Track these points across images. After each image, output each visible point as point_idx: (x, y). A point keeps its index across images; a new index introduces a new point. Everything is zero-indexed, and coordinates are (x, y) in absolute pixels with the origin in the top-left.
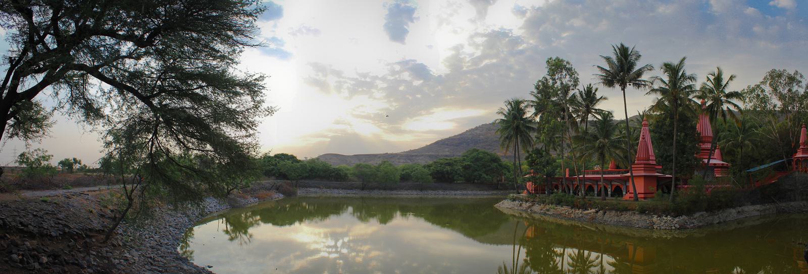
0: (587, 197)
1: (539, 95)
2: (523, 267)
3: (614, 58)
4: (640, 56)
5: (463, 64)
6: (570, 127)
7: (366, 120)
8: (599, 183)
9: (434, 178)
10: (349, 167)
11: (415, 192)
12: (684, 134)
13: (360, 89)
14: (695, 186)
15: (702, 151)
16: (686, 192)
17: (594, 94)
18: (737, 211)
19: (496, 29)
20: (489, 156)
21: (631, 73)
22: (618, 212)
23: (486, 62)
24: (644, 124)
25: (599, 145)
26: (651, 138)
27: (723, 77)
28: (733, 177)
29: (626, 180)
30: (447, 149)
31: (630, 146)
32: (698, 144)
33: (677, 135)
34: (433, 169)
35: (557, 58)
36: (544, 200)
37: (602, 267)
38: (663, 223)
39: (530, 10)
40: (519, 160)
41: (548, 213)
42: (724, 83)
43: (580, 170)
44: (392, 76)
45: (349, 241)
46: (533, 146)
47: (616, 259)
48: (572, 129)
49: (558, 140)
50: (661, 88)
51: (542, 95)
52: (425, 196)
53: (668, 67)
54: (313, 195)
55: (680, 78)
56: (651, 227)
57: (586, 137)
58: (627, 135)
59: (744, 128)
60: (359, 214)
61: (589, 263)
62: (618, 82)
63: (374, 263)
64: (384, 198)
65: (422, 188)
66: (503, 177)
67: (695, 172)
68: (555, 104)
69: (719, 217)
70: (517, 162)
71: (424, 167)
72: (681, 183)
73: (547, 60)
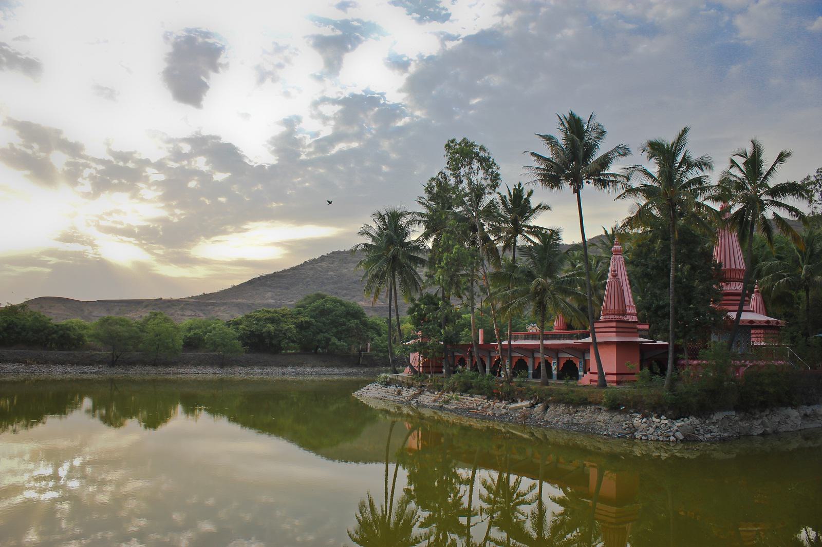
0: (515, 380)
1: (432, 203)
2: (402, 501)
3: (560, 138)
4: (604, 132)
5: (301, 149)
6: (485, 258)
7: (125, 238)
8: (536, 355)
9: (245, 345)
10: (87, 324)
11: (210, 370)
12: (690, 266)
13: (116, 181)
14: (714, 363)
15: (725, 298)
16: (696, 371)
17: (527, 200)
18: (803, 413)
19: (359, 92)
20: (343, 307)
21: (590, 162)
22: (571, 407)
23: (341, 146)
24: (615, 251)
25: (535, 288)
26: (629, 275)
27: (762, 157)
28: (791, 347)
29: (583, 350)
30: (269, 294)
31: (591, 290)
32: (717, 285)
33: (676, 270)
34: (244, 329)
35: (465, 141)
36: (440, 384)
37: (541, 503)
38: (652, 428)
39: (415, 61)
40: (398, 315)
41: (446, 406)
42: (765, 168)
43: (503, 333)
44: (175, 161)
45: (83, 465)
46: (421, 290)
47: (565, 492)
48: (488, 260)
49: (466, 279)
50: (645, 185)
51: (437, 203)
52: (230, 377)
53: (656, 149)
54: (9, 378)
55: (680, 166)
56: (630, 435)
57: (515, 275)
58: (584, 270)
59: (812, 251)
60: (104, 412)
61: (518, 496)
62: (567, 179)
63: (132, 504)
64: (154, 381)
65: (222, 363)
66: (369, 344)
67: (713, 335)
68: (460, 218)
69: (763, 423)
70: (394, 318)
71: (228, 324)
72: (686, 356)
73: (447, 143)
